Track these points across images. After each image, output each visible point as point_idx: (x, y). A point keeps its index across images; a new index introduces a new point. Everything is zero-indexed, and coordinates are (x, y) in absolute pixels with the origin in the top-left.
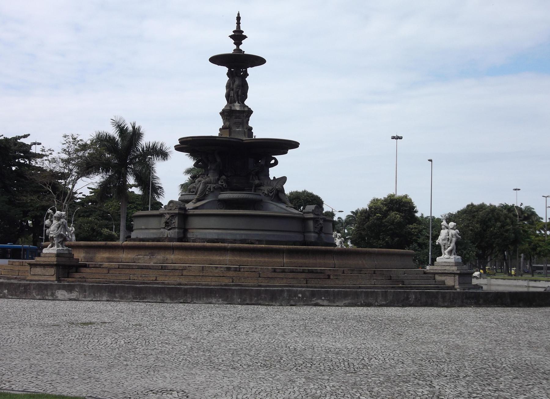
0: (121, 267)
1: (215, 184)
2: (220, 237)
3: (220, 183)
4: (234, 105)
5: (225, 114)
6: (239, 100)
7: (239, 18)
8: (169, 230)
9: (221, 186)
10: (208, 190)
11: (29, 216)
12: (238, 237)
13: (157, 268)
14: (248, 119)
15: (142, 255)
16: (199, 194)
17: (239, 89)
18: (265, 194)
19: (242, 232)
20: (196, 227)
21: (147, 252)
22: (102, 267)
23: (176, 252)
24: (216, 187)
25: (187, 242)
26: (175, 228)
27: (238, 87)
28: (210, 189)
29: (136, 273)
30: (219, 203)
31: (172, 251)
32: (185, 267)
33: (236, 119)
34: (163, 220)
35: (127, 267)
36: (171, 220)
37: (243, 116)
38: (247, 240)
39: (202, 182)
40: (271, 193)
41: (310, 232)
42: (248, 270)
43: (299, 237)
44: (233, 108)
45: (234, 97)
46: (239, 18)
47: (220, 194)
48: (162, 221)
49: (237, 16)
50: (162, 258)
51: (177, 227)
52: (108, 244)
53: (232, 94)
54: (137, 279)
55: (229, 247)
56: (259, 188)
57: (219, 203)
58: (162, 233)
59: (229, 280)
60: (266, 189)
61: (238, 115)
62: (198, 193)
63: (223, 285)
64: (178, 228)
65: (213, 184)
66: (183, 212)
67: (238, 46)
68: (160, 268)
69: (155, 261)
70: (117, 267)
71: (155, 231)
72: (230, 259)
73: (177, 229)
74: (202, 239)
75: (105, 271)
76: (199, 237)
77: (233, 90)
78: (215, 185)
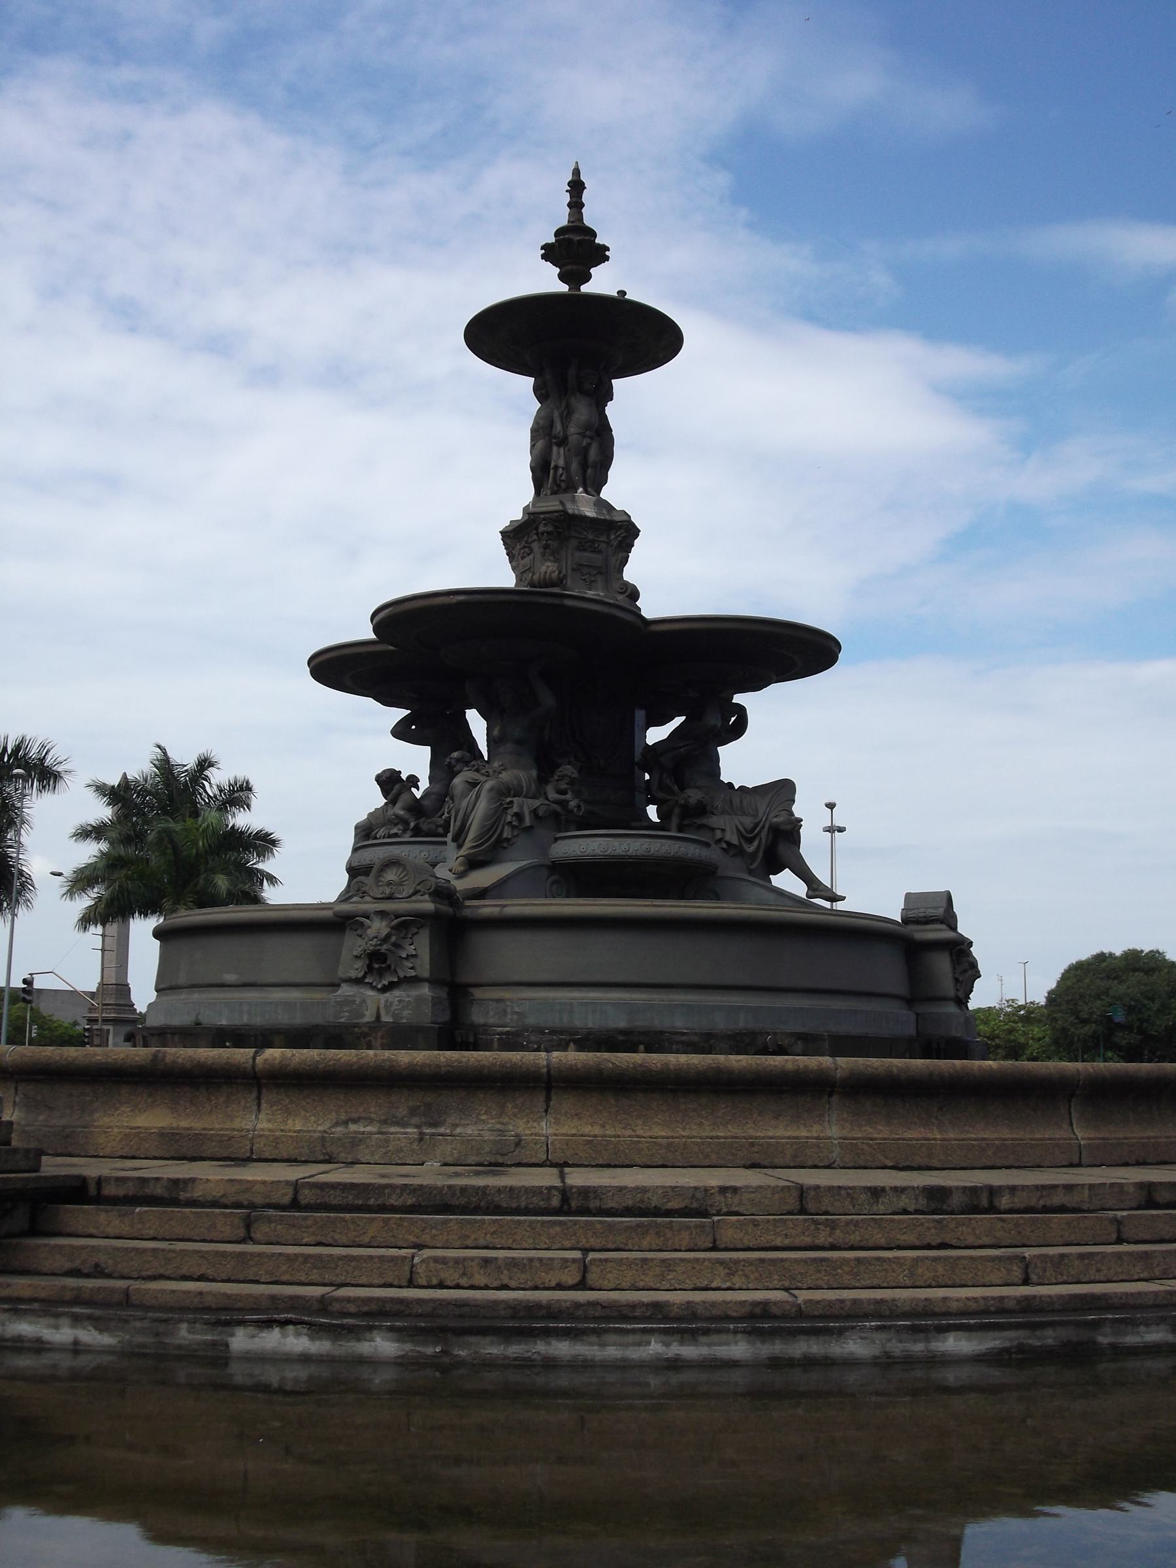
0: (306, 1197)
1: (534, 797)
2: (641, 1022)
3: (553, 795)
4: (574, 500)
5: (542, 528)
6: (588, 482)
7: (577, 187)
8: (385, 989)
9: (558, 808)
10: (510, 823)
11: (220, 821)
12: (721, 1024)
13: (537, 1201)
14: (625, 554)
15: (370, 1121)
16: (476, 839)
17: (591, 438)
18: (728, 843)
19: (736, 999)
20: (517, 978)
21: (403, 1104)
22: (183, 1196)
23: (565, 1102)
24: (541, 813)
25: (476, 1048)
26: (414, 981)
27: (588, 433)
28: (519, 816)
29: (426, 1238)
30: (552, 878)
31: (542, 1098)
32: (699, 1195)
33: (585, 550)
34: (353, 945)
35: (350, 1199)
36: (397, 945)
37: (608, 543)
38: (761, 1033)
39: (488, 786)
40: (750, 841)
41: (944, 999)
42: (1033, 1203)
43: (901, 1023)
44: (570, 508)
45: (567, 468)
46: (577, 187)
47: (556, 839)
48: (344, 952)
49: (570, 178)
50: (487, 1136)
51: (426, 974)
52: (168, 1059)
53: (558, 457)
54: (463, 1281)
55: (839, 1074)
56: (699, 821)
57: (552, 878)
58: (348, 1002)
59: (1009, 1271)
60: (728, 826)
61: (590, 537)
62: (471, 835)
63: (1011, 1304)
64: (433, 982)
65: (526, 797)
66: (445, 908)
67: (575, 273)
68: (555, 1202)
69: (448, 1150)
70: (286, 1200)
71: (295, 995)
72: (845, 1133)
73: (426, 985)
74: (553, 1032)
75: (227, 1222)
76: (532, 1020)
77: (563, 442)
78: (536, 803)
